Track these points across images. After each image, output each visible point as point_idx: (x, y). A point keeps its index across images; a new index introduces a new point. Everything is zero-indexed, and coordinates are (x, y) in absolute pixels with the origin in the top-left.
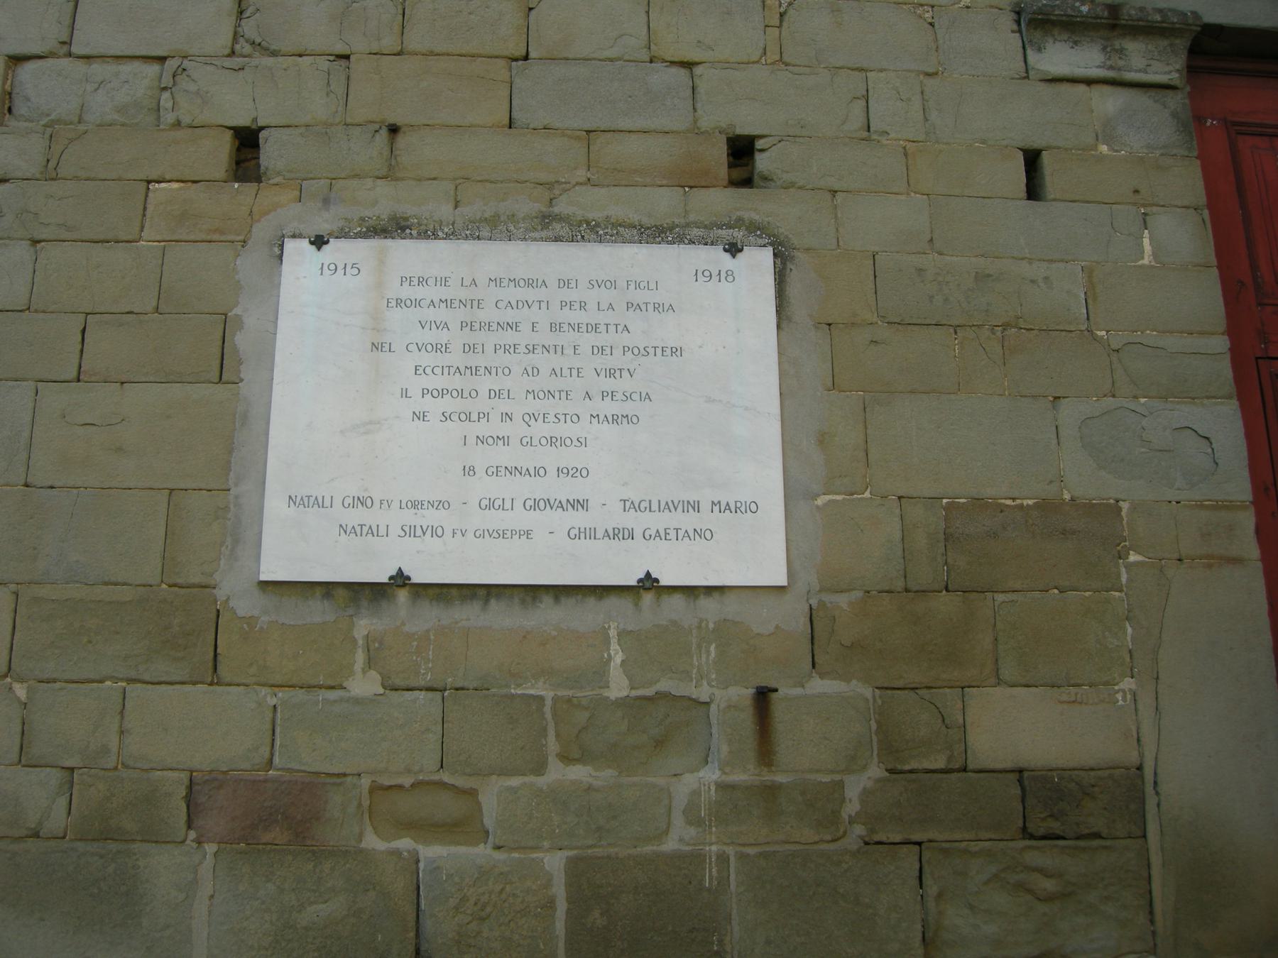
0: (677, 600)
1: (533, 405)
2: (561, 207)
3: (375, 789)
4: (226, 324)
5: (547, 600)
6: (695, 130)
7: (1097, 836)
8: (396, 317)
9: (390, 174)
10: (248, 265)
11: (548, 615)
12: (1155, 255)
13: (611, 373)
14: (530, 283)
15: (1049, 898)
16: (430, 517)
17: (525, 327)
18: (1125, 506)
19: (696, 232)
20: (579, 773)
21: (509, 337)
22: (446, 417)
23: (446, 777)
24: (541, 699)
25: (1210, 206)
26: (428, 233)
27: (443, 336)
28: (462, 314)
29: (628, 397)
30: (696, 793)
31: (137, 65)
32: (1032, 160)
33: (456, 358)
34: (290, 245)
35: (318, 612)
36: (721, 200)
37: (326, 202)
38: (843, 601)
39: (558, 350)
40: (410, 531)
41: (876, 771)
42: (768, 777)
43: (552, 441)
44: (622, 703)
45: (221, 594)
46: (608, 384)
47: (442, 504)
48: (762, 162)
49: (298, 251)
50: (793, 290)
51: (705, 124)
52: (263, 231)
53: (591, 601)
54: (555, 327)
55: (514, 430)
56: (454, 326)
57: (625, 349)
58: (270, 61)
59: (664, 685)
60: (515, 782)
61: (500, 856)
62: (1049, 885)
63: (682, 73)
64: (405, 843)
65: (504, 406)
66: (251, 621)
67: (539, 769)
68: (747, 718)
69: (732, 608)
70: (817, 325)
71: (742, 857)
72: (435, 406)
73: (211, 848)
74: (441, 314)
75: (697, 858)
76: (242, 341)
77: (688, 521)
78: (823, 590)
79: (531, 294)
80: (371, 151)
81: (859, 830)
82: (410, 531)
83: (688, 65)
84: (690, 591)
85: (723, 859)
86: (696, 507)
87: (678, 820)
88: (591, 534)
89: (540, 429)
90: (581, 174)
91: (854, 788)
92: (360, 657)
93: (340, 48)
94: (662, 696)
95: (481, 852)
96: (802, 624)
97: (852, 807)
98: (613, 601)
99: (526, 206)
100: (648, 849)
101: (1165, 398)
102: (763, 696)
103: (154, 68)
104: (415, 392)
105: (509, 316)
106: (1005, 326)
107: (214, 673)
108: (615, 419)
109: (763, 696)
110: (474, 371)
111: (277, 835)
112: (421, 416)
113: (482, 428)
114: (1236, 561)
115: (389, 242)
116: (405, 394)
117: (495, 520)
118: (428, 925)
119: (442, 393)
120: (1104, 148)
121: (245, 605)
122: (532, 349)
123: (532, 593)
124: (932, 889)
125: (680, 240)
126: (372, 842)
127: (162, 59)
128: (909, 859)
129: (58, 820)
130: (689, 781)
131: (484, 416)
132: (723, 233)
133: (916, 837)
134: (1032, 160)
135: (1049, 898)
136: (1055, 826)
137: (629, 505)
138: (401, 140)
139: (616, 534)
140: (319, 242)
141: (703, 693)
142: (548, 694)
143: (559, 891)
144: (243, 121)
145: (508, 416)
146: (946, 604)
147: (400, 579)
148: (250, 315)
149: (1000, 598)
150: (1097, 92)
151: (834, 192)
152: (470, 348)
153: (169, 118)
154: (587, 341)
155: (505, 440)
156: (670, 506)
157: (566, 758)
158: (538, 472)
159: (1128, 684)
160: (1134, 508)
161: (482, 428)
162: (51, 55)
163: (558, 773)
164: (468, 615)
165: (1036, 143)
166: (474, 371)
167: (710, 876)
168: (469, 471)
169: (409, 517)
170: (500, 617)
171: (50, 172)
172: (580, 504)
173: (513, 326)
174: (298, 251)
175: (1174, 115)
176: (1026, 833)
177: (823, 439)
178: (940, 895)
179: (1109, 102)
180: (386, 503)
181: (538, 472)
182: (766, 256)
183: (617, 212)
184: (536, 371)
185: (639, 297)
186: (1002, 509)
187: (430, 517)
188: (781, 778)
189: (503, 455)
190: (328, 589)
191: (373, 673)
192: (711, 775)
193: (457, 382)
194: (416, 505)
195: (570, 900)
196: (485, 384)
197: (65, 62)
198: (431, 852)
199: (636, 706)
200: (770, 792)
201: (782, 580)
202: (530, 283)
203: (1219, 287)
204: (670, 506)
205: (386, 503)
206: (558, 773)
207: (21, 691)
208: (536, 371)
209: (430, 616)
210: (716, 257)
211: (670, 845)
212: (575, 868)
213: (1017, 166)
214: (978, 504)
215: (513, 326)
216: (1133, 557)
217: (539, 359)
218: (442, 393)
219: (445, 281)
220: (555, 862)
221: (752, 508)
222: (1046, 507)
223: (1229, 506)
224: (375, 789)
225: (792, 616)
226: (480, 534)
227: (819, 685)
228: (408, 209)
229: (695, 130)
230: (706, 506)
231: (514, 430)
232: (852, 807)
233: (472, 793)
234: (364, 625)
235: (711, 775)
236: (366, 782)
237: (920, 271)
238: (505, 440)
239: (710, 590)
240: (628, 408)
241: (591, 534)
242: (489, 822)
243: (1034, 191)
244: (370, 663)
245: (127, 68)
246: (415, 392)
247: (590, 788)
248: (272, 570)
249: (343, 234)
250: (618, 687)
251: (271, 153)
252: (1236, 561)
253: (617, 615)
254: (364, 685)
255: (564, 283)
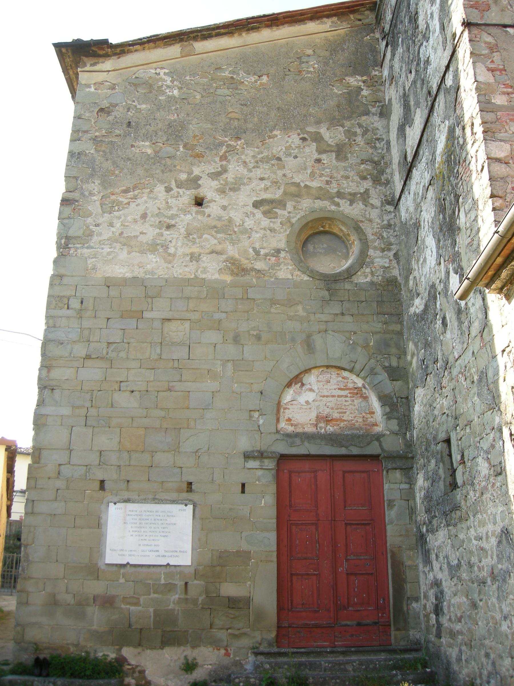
0: (173, 568)
1: (151, 534)
2: (157, 497)
3: (124, 598)
4: (99, 518)
5: (152, 567)
6: (181, 481)
7: (241, 608)
8: (128, 518)
9: (128, 489)
10: (103, 507)
11: (152, 570)
12: (264, 504)
13: (164, 528)
14: (151, 511)
15: (232, 618)
16: (133, 553)
17: (150, 520)
18: (252, 551)
19: (180, 501)
20: (156, 595)
21: (147, 521)
22: (136, 536)
23: (135, 596)
24: (150, 583)
25: (277, 493)
26: (134, 502)
27: (136, 521)
28: (139, 517)
29: (166, 532)
30: (174, 599)
31: (82, 467)
32: (243, 485)
33: (138, 525)
34: (110, 504)
35: (115, 569)
36: (185, 495)
37: (116, 495)
38: (201, 568)
39: (155, 524)
40: (130, 555)
41: (204, 596)
42: (186, 597)
43: (153, 540)
44: (164, 584)
45: (99, 565)
46: (163, 530)
47: (135, 551)
48: (193, 487)
49: (111, 505)
50: (196, 512)
51: (183, 480)
52: (105, 501)
53: (159, 567)
54: (155, 520)
55: (147, 538)
56: (138, 519)
57: (167, 524)
58: (106, 466)
59: (170, 581)
60: (146, 597)
61: (143, 609)
62: (232, 616)
63: (180, 469)
64: (128, 606)
65: (146, 534)
66: (104, 570)
67: (150, 594)
68: (184, 587)
69: (128, 569)
70: (200, 519)
71: (181, 610)
72: (134, 534)
73: (97, 607)
74: (135, 517)
75: (174, 610)
76: (102, 521)
77: (175, 554)
78: (198, 566)
79: (151, 514)
80: (123, 485)
81: (201, 606)
82: (130, 555)
83: (181, 468)
84: (175, 566)
85: (178, 610)
86: (177, 551)
87: (171, 603)
88: (159, 556)
89: (152, 538)
90: (161, 490)
91: (200, 599)
92: (121, 576)
93: (119, 464)
94: (170, 583)
95: (140, 608)
96: (193, 572)
97: (200, 602)
98: (162, 567)
99: (151, 497)
100: (167, 608)
101: (262, 531)
102: (186, 584)
103: (85, 468)
104: (131, 531)
105: (147, 518)
106: (234, 518)
107: (98, 578)
108: (164, 536)
109: (186, 584)
110: (141, 527)
111: (108, 605)
112: (132, 535)
113: (142, 538)
114: (272, 561)
115: (127, 504)
116: (129, 531)
117: (143, 553)
118: (131, 620)
119: (136, 531)
120: (257, 482)
121: (103, 567)
122: (151, 524)
123: (149, 566)
124: (212, 616)
125: (177, 503)
126: (123, 606)
127: (87, 466)
128: (209, 611)
129: (72, 602)
130: (173, 597)
131: (142, 535)
132: (185, 501)
133: (210, 607)
134: (243, 485)
135: (232, 618)
136: (234, 606)
137: (166, 551)
138: (130, 483)
139: (163, 556)
140: (115, 504)
141: (176, 583)
142: (151, 583)
143: (152, 615)
144: (102, 479)
145: (146, 536)
146: (218, 568)
147: (128, 563)
148: (103, 516)
149: (228, 567)
150: (257, 471)
151: (205, 493)
152: (140, 523)
153: (88, 478)
154: (160, 522)
155: (146, 540)
156: (173, 551)
157: (154, 593)
158: (151, 545)
159: (249, 583)
160: (254, 552)
161: (142, 538)
162: (66, 464)
163: (153, 596)
164: (139, 569)
165: (244, 482)
166: (141, 527)
167: (176, 613)
168: (140, 545)
169: (130, 553)
170: (144, 570)
171: (68, 488)
172: (157, 551)
173: (148, 519)
174: (111, 505)
175: (273, 475)
176: (229, 607)
177: (199, 540)
178: (213, 617)
179: (260, 473)
180: (126, 551)
181: (151, 545)
182: (192, 506)
183: (166, 498)
184: (151, 528)
185: (169, 514)
186: (230, 552)
187: (133, 553)
188: (189, 597)
189: (145, 542)
190: (116, 565)
191: (124, 579)
192: (177, 596)
193: (138, 529)
194: (131, 551)
195: (154, 616)
196: (143, 530)
197: (69, 466)
198: (132, 608)
199: (166, 585)
200: (187, 599)
201: (190, 564)
202: (151, 511)
203: (276, 510)
204: (173, 551)
205: (126, 551)
206: (153, 596)
207: (66, 581)
208: (151, 528)
209: (132, 570)
210: (183, 506)
211: (170, 607)
212: (155, 611)
213: (240, 486)
214: (226, 551)
215: (148, 519)
216: (253, 561)
217: (152, 525)
218: (136, 531)
219: (136, 511)
220: (151, 610)
221: (186, 552)
222: (238, 552)
223: (272, 551)
224: (124, 598)
225: (192, 570)
226: (141, 556)
227: (196, 582)
228: (130, 497)
229: (181, 481)
230: (178, 551)
231: (147, 538)
232: (200, 602)
233: (139, 599)
234: (122, 571)
235: (177, 596)
236: (122, 597)
237: (219, 508)
238: (146, 540)
239: (178, 566)
240: (166, 534)
241: (159, 556)
242: (141, 603)
243: (243, 492)
244: (123, 577)
245: (80, 467)
246: (131, 531)
247: (158, 598)
248: (108, 561)
249: (119, 502)
250: (163, 582)
251: (107, 485)
252: (272, 561)
253: (163, 570)
254: (122, 581)
255: (157, 512)
